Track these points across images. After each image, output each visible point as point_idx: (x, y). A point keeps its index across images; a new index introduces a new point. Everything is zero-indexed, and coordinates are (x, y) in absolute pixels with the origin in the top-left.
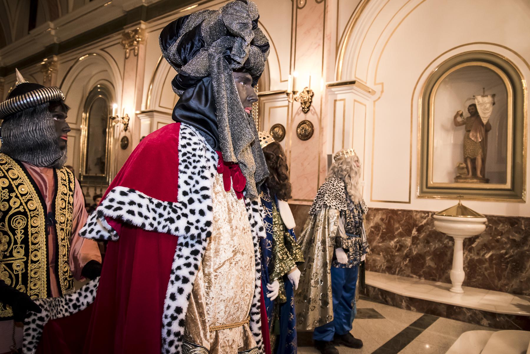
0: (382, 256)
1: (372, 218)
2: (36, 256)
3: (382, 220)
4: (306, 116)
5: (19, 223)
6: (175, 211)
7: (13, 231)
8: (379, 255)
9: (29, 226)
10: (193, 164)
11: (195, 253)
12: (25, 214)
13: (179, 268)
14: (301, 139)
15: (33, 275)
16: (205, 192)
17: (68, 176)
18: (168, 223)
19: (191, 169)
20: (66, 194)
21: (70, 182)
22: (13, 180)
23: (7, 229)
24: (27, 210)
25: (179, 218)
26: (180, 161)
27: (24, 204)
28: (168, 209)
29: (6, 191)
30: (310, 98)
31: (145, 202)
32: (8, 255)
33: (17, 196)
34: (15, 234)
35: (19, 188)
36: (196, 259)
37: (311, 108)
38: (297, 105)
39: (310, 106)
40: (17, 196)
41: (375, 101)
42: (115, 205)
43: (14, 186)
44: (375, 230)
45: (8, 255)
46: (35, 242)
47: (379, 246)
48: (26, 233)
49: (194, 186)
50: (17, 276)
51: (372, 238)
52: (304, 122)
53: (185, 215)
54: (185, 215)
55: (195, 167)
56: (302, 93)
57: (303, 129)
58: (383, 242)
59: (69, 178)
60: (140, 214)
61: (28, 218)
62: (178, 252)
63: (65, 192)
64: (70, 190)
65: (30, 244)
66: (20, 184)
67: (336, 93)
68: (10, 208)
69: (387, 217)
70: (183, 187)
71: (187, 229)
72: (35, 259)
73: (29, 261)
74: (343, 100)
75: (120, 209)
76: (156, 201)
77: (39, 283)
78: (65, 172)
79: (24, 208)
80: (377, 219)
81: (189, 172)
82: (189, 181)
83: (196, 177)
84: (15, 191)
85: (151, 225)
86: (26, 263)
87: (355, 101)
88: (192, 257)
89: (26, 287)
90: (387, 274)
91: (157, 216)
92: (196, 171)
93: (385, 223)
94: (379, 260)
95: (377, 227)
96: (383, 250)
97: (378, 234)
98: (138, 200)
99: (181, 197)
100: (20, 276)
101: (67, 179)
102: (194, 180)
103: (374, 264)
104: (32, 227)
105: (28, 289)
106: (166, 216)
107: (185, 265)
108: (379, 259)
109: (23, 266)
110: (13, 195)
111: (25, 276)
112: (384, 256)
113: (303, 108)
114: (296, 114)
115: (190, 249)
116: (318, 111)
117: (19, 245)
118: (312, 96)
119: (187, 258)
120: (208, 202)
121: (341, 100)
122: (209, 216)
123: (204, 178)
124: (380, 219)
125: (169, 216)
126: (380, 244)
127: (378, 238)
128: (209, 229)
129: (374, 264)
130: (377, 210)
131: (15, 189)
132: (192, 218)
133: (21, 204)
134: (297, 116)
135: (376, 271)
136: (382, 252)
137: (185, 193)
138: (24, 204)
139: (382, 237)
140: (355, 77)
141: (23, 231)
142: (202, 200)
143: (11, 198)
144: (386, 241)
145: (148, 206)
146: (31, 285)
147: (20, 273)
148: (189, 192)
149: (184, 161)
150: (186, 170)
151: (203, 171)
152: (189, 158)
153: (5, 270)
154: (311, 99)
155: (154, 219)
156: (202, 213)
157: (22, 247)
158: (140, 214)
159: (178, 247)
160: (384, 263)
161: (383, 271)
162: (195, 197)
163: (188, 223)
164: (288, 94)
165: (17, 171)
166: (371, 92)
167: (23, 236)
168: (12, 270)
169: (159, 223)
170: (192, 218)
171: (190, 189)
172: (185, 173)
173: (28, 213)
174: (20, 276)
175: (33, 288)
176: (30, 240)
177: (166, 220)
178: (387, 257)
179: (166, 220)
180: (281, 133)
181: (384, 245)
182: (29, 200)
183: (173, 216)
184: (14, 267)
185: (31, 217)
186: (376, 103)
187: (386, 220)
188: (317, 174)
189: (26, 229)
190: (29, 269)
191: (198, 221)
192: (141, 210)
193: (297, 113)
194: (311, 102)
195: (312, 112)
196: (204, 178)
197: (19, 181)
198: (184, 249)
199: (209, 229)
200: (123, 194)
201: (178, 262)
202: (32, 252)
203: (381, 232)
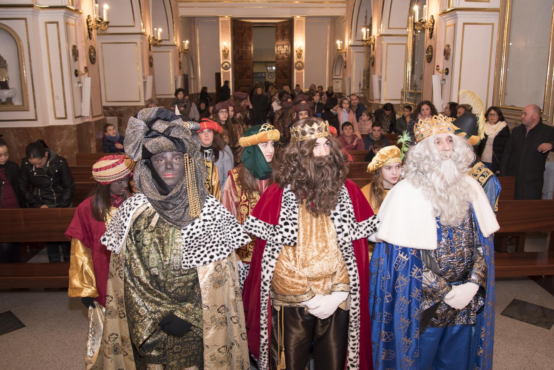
6: (275, 230)
10: (289, 204)
11: (274, 250)
13: (265, 256)
16: (294, 221)
18: (272, 236)
19: (288, 207)
25: (277, 234)
26: (282, 201)
28: (273, 229)
31: (262, 225)
36: (273, 253)
42: (250, 227)
49: (289, 216)
53: (281, 233)
54: (281, 233)
55: (290, 206)
60: (259, 232)
62: (266, 248)
70: (282, 216)
71: (283, 240)
75: (251, 229)
76: (267, 224)
81: (287, 208)
82: (286, 213)
83: (290, 212)
85: (264, 237)
91: (267, 233)
92: (290, 208)
98: (259, 225)
99: (281, 223)
102: (289, 213)
106: (271, 233)
107: (268, 255)
115: (272, 248)
119: (270, 252)
120: (296, 227)
122: (296, 234)
123: (295, 213)
125: (272, 233)
128: (295, 241)
132: (286, 234)
137: (283, 219)
142: (293, 225)
145: (263, 228)
148: (286, 218)
149: (285, 201)
150: (285, 206)
151: (294, 209)
152: (287, 200)
155: (266, 234)
156: (292, 232)
158: (259, 232)
159: (267, 246)
162: (290, 222)
163: (283, 236)
169: (268, 237)
170: (286, 234)
171: (287, 218)
172: (284, 208)
177: (271, 235)
179: (271, 235)
183: (275, 233)
191: (289, 236)
192: (259, 229)
196: (295, 213)
198: (269, 247)
199: (295, 241)
200: (253, 221)
201: (265, 253)
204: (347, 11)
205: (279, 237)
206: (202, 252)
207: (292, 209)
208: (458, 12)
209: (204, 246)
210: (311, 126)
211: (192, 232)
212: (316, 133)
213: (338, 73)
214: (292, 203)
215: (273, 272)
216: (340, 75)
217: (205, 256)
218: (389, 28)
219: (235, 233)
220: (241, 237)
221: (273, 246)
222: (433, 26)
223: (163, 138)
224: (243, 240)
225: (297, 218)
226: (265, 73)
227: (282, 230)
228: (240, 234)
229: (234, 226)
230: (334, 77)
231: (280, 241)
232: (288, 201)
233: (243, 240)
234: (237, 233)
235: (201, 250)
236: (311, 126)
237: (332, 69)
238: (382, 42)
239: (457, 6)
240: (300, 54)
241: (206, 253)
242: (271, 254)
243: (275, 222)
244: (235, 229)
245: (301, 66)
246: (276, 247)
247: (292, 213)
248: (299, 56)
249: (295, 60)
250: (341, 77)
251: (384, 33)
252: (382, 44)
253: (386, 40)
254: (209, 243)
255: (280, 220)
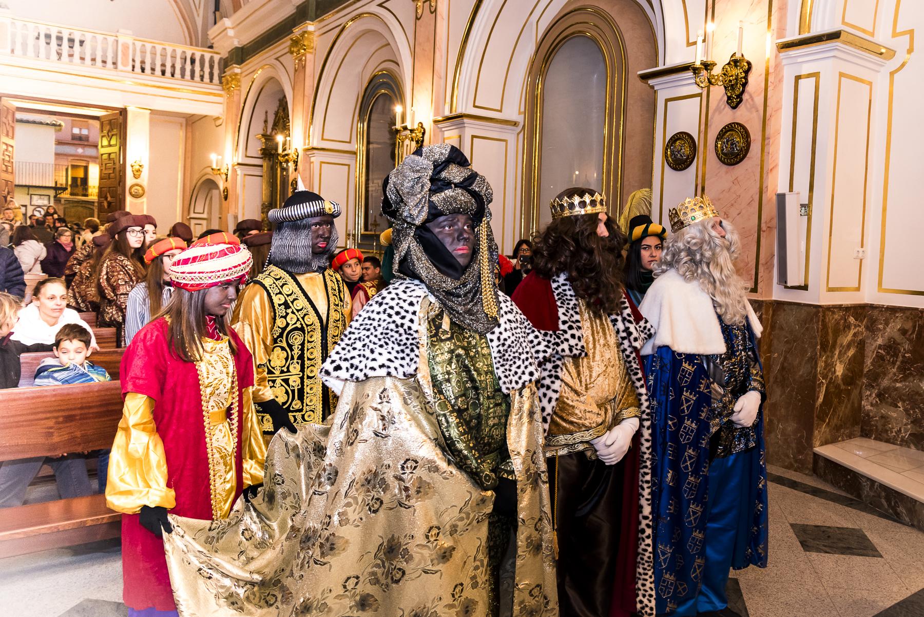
0: (901, 409)
1: (881, 326)
2: (312, 371)
3: (903, 332)
4: (734, 113)
5: (296, 339)
6: (559, 338)
7: (290, 346)
8: (897, 406)
9: (306, 342)
10: (567, 302)
11: (556, 367)
12: (302, 329)
14: (724, 162)
15: (309, 391)
16: (578, 324)
17: (338, 284)
20: (338, 305)
21: (340, 292)
22: (288, 295)
23: (284, 345)
24: (304, 325)
25: (562, 342)
27: (301, 319)
29: (283, 307)
30: (743, 75)
32: (286, 370)
33: (293, 312)
34: (292, 350)
35: (295, 303)
37: (745, 97)
38: (718, 92)
39: (743, 91)
40: (293, 312)
41: (892, 74)
43: (289, 302)
44: (888, 353)
45: (286, 370)
46: (311, 357)
47: (896, 389)
48: (302, 350)
50: (293, 391)
51: (880, 370)
52: (730, 128)
53: (567, 340)
54: (567, 340)
55: (568, 304)
56: (727, 66)
57: (728, 141)
58: (904, 379)
59: (339, 287)
61: (304, 334)
63: (337, 303)
64: (341, 300)
65: (306, 359)
66: (295, 300)
67: (800, 60)
68: (288, 324)
69: (914, 327)
70: (563, 318)
72: (311, 375)
73: (305, 377)
74: (816, 75)
77: (314, 399)
78: (335, 281)
79: (301, 324)
80: (893, 329)
83: (571, 312)
84: (290, 307)
86: (302, 379)
87: (842, 75)
88: (648, 333)
89: (302, 403)
90: (913, 450)
92: (570, 306)
93: (910, 340)
94: (896, 419)
95: (891, 347)
96: (905, 398)
97: (894, 363)
100: (296, 391)
101: (337, 289)
103: (884, 425)
104: (308, 342)
105: (305, 404)
108: (895, 415)
109: (299, 381)
110: (289, 311)
111: (301, 392)
112: (906, 410)
113: (729, 98)
114: (715, 111)
115: (552, 364)
116: (759, 100)
117: (295, 361)
118: (747, 72)
119: (550, 371)
121: (809, 76)
124: (899, 330)
126: (898, 385)
127: (894, 370)
129: (884, 425)
130: (893, 310)
131: (291, 305)
132: (573, 342)
133: (298, 320)
134: (717, 113)
135: (888, 441)
136: (904, 401)
137: (564, 322)
138: (301, 319)
139: (902, 369)
140: (844, 22)
141: (300, 347)
143: (287, 314)
144: (911, 379)
146: (306, 401)
147: (296, 389)
149: (559, 299)
153: (274, 368)
154: (746, 78)
157: (298, 363)
160: (906, 425)
161: (904, 443)
164: (696, 71)
165: (291, 286)
166: (882, 53)
167: (300, 352)
168: (289, 385)
170: (573, 342)
173: (306, 329)
174: (296, 391)
175: (309, 404)
176: (305, 356)
177: (553, 344)
178: (914, 412)
180: (686, 151)
181: (907, 386)
182: (305, 315)
183: (559, 341)
184: (291, 382)
185: (308, 332)
186: (896, 75)
187: (913, 332)
188: (756, 235)
189: (303, 344)
190: (305, 384)
193: (718, 110)
194: (744, 85)
195: (748, 106)
197: (293, 297)
202: (308, 367)
203: (900, 358)
204: (228, 109)
205: (565, 346)
206: (519, 367)
207: (572, 309)
208: (466, 120)
209: (519, 359)
210: (582, 198)
211: (502, 338)
212: (599, 206)
213: (199, 208)
214: (571, 300)
215: (557, 399)
216: (203, 213)
217: (523, 373)
218: (323, 139)
219: (532, 342)
220: (541, 348)
221: (554, 362)
222: (423, 137)
223: (459, 191)
224: (545, 351)
225: (579, 319)
226: (25, 206)
227: (568, 336)
228: (539, 343)
229: (530, 331)
230: (193, 215)
231: (567, 352)
232: (564, 298)
233: (545, 351)
234: (536, 341)
235: (517, 365)
236: (582, 198)
237: (187, 203)
238: (312, 159)
239: (464, 112)
240: (138, 171)
241: (522, 368)
242: (553, 373)
243: (555, 328)
244: (531, 337)
245: (141, 192)
246: (559, 363)
247: (574, 314)
248: (137, 174)
249: (130, 180)
250: (205, 216)
251: (315, 145)
252: (311, 163)
253: (316, 158)
254: (394, 322)
255: (560, 323)
